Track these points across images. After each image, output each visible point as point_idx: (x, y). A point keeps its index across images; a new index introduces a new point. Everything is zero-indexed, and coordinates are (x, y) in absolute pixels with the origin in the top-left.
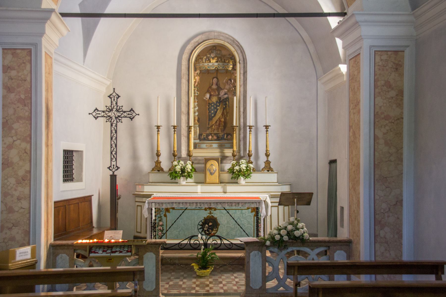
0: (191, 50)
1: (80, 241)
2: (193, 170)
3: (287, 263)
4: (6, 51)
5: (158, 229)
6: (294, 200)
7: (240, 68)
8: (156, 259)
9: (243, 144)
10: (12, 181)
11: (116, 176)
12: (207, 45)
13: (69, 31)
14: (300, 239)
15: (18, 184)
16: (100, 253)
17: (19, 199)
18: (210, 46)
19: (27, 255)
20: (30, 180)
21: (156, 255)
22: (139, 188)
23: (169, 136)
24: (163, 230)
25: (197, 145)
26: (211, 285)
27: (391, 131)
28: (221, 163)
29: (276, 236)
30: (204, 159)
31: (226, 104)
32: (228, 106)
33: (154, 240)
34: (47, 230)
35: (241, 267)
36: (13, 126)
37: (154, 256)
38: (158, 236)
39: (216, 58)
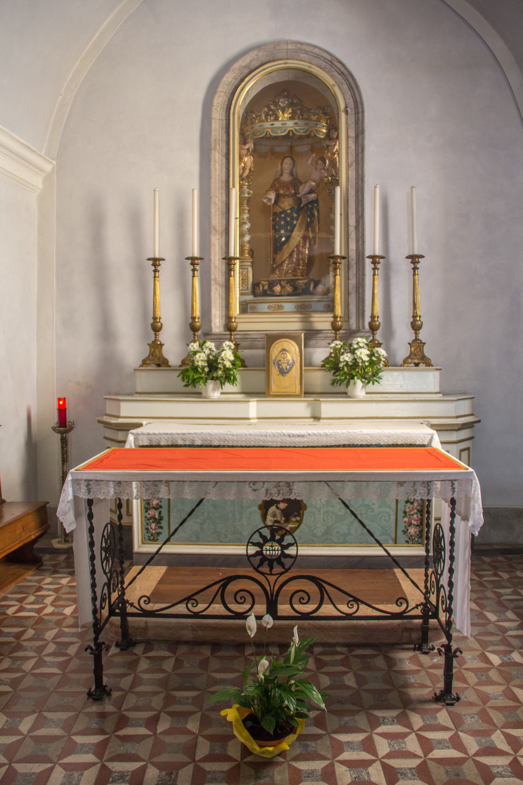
0: (234, 87)
2: (238, 363)
5: (149, 516)
7: (347, 123)
9: (355, 302)
22: (110, 408)
24: (161, 519)
25: (249, 305)
28: (305, 347)
30: (264, 336)
31: (312, 215)
32: (316, 219)
38: (149, 535)
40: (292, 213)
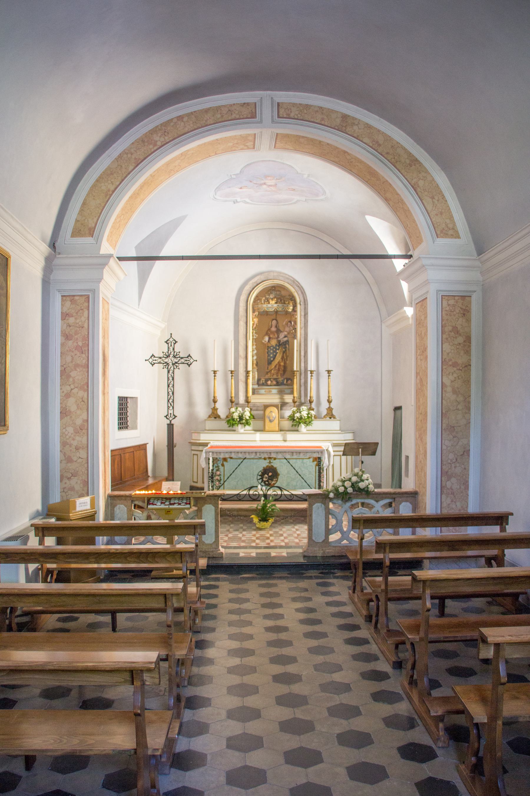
1: (138, 492)
2: (252, 417)
3: (352, 516)
4: (64, 298)
6: (359, 450)
7: (300, 309)
8: (215, 512)
10: (70, 430)
11: (173, 425)
12: (266, 285)
13: (126, 275)
14: (365, 491)
15: (76, 433)
16: (159, 505)
17: (77, 449)
18: (269, 287)
19: (86, 505)
20: (88, 430)
21: (215, 507)
22: (194, 436)
23: (226, 382)
24: (221, 480)
25: (256, 391)
26: (272, 538)
27: (459, 379)
29: (340, 487)
31: (285, 348)
33: (211, 492)
34: (105, 480)
35: (303, 519)
36: (71, 374)
37: (213, 508)
39: (275, 299)
40: (276, 347)
